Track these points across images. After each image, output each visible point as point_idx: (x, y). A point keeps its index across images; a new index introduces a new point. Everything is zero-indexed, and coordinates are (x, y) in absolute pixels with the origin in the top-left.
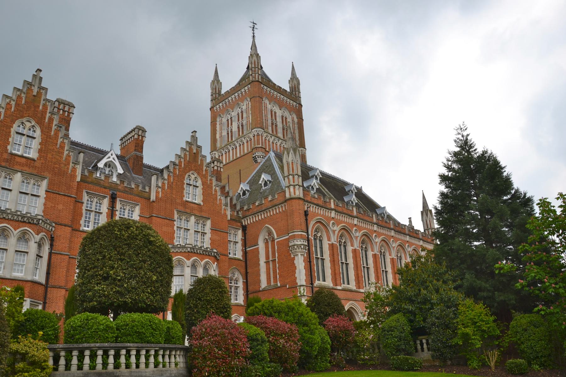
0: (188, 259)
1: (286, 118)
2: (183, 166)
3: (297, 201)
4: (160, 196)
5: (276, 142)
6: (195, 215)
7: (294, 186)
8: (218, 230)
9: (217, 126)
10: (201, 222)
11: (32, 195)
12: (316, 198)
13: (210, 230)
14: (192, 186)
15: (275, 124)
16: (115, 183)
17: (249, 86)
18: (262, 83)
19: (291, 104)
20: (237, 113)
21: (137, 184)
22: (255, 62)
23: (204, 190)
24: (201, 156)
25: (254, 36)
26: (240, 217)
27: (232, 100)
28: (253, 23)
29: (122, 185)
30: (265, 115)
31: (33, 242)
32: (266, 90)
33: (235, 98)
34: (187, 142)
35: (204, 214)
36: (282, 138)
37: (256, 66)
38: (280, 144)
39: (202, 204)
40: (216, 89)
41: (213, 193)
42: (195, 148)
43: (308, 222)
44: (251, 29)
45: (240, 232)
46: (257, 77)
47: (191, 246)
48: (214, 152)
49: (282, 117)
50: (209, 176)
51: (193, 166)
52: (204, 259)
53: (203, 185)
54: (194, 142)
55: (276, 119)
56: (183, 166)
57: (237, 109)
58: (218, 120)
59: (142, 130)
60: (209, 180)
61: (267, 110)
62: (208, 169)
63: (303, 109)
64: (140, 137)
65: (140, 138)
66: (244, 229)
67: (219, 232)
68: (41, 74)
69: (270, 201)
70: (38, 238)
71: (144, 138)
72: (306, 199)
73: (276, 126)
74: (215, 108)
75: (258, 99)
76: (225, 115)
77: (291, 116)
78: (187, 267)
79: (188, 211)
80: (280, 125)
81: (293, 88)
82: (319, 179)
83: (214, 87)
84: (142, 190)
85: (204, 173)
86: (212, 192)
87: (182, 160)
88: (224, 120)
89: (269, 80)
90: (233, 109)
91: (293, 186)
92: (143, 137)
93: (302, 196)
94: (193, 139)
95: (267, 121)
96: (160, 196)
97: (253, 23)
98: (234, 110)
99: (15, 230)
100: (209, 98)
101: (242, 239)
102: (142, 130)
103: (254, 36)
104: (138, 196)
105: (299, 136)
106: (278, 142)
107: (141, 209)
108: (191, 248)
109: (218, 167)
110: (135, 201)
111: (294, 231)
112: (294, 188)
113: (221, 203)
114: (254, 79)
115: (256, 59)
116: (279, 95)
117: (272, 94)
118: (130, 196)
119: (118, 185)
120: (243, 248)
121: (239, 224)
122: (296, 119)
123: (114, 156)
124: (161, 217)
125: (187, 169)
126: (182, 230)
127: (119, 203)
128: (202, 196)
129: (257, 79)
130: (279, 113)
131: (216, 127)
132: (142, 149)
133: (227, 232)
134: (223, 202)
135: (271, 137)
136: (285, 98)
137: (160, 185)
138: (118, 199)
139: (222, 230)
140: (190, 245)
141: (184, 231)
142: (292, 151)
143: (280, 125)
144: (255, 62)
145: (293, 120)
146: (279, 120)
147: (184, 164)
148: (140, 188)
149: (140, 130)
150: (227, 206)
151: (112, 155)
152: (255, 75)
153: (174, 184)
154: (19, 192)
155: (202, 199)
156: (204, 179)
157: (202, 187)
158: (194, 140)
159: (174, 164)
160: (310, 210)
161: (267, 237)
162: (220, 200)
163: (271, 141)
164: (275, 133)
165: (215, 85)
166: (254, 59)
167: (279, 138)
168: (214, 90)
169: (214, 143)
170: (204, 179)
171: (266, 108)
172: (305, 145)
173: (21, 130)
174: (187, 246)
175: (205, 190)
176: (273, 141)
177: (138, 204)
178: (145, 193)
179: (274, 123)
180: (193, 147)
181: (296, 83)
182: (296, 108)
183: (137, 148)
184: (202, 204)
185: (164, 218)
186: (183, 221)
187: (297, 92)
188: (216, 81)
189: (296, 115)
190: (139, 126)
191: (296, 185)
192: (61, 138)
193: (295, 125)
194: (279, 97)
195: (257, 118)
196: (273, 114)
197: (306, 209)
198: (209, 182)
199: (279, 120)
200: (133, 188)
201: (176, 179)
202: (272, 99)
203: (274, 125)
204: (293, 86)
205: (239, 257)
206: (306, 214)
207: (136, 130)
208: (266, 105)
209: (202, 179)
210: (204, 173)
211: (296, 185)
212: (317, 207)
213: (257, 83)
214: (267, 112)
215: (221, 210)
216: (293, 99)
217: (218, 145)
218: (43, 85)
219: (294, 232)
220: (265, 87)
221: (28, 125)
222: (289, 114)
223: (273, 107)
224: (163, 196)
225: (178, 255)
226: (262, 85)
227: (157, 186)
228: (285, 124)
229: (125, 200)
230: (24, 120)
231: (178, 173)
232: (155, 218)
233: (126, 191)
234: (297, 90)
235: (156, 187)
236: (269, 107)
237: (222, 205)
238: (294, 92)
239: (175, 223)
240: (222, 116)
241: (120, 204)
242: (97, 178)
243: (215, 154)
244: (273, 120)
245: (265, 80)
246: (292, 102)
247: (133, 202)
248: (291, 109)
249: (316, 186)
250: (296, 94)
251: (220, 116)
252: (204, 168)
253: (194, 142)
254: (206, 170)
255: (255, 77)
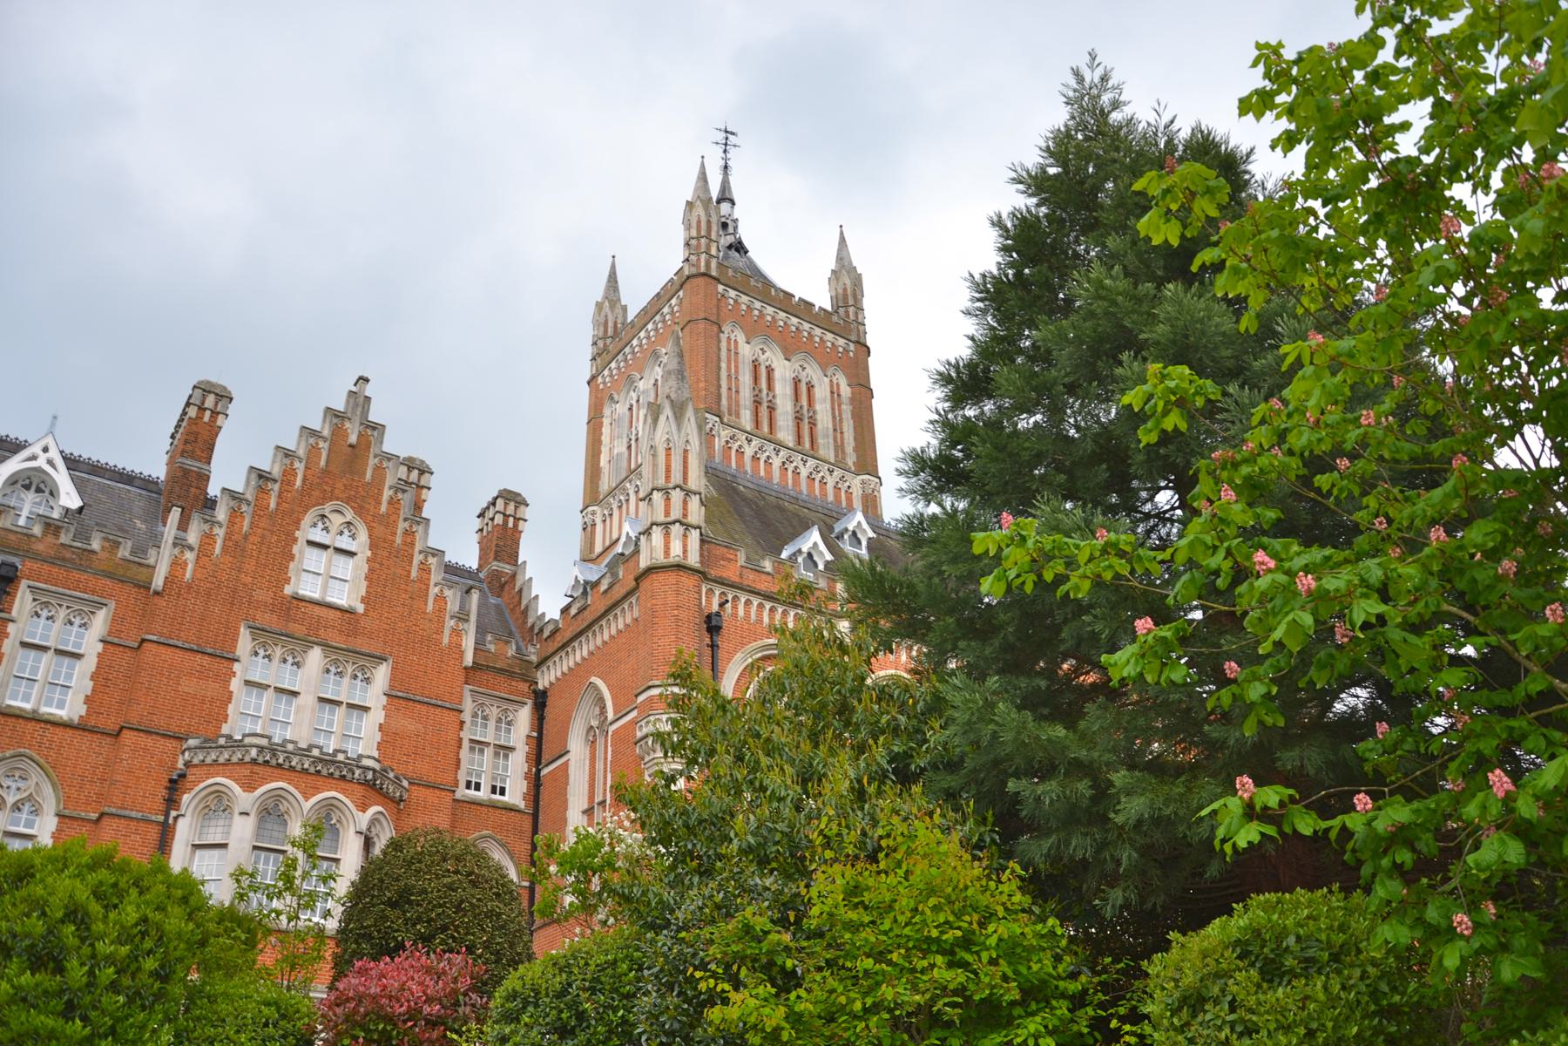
0: (249, 787)
1: (810, 387)
2: (298, 483)
3: (671, 577)
4: (188, 575)
5: (768, 457)
6: (325, 646)
7: (666, 526)
8: (418, 698)
9: (604, 430)
10: (350, 670)
11: (59, 652)
12: (768, 574)
13: (385, 698)
14: (331, 551)
15: (765, 405)
16: (25, 531)
17: (681, 293)
18: (718, 280)
19: (829, 344)
20: (653, 381)
21: (111, 537)
22: (699, 222)
23: (377, 566)
24: (375, 456)
25: (726, 167)
26: (530, 662)
27: (641, 345)
28: (726, 132)
29: (50, 539)
30: (729, 376)
31: (352, 830)
32: (760, 311)
33: (648, 338)
34: (329, 412)
35: (361, 644)
36: (791, 445)
37: (703, 233)
38: (784, 463)
39: (360, 608)
40: (606, 323)
41: (414, 574)
42: (356, 431)
43: (721, 654)
44: (720, 149)
45: (524, 717)
46: (703, 264)
47: (264, 742)
48: (590, 509)
49: (796, 382)
50: (401, 519)
51: (339, 485)
52: (317, 790)
53: (373, 546)
54: (354, 412)
55: (770, 387)
56: (298, 483)
57: (653, 369)
58: (607, 411)
59: (217, 395)
60: (399, 532)
61: (736, 361)
62: (400, 496)
63: (873, 362)
64: (511, 519)
65: (511, 524)
66: (540, 701)
67: (424, 708)
68: (369, 390)
69: (606, 592)
70: (363, 819)
71: (220, 416)
72: (713, 573)
73: (772, 409)
74: (600, 380)
75: (702, 325)
76: (623, 394)
77: (827, 380)
78: (241, 813)
79: (298, 629)
80: (785, 406)
81: (840, 297)
82: (864, 543)
83: (602, 320)
84: (132, 558)
85: (383, 508)
86: (409, 572)
87: (299, 467)
88: (621, 409)
89: (768, 283)
90: (641, 371)
91: (660, 528)
92: (218, 413)
93: (693, 559)
94: (352, 401)
95: (737, 392)
96: (188, 575)
97: (726, 132)
98: (646, 374)
99: (307, 799)
100: (589, 351)
101: (528, 736)
102: (217, 395)
103: (726, 167)
104: (109, 575)
105: (855, 439)
106: (773, 455)
107: (115, 620)
108: (261, 749)
109: (506, 516)
110: (93, 592)
111: (650, 683)
112: (667, 535)
113: (440, 610)
114: (694, 270)
115: (702, 214)
116: (782, 315)
117: (756, 312)
118: (76, 575)
119: (33, 540)
120: (530, 770)
121: (524, 687)
122: (848, 389)
123: (54, 454)
124: (180, 644)
125: (316, 493)
126: (489, 752)
127: (31, 598)
128: (365, 584)
129: (703, 270)
130: (784, 370)
131: (601, 434)
132: (212, 451)
133: (455, 707)
134: (453, 605)
135: (749, 441)
136: (806, 326)
137: (193, 537)
138: (24, 583)
139: (433, 701)
140: (262, 736)
141: (497, 754)
142: (667, 411)
143: (785, 406)
144: (699, 222)
145: (835, 393)
146: (783, 391)
147: (305, 479)
148: (124, 552)
149: (210, 392)
150: (467, 621)
151: (45, 450)
152: (699, 260)
153: (251, 539)
154: (18, 644)
155: (363, 592)
156: (382, 528)
157: (369, 553)
158: (357, 405)
159: (260, 477)
160: (735, 615)
161: (594, 723)
162: (440, 598)
163: (804, 472)
164: (807, 445)
165: (603, 314)
166: (841, 283)
167: (780, 445)
168: (602, 329)
169: (592, 482)
170: (380, 530)
171: (736, 353)
172: (876, 467)
173: (318, 535)
174: (247, 740)
175: (381, 564)
176: (756, 453)
177: (104, 601)
178: (141, 569)
179: (765, 400)
180: (347, 425)
181: (848, 282)
182: (848, 356)
183: (189, 447)
184: (360, 608)
185: (191, 650)
186: (492, 724)
187: (851, 310)
188: (607, 303)
189: (848, 376)
190: (208, 382)
191: (674, 522)
192: (436, 585)
193: (844, 407)
194: (781, 323)
195: (698, 381)
196: (762, 375)
197: (715, 607)
198: (398, 540)
199: (783, 391)
200: (93, 552)
201: (264, 523)
202: (756, 329)
203: (763, 406)
204: (840, 291)
205: (512, 801)
206: (712, 626)
207: (500, 503)
208: (736, 347)
209: (370, 529)
210: (383, 508)
211: (674, 522)
212: (768, 605)
213: (701, 281)
214: (736, 367)
215: (440, 632)
216: (833, 329)
217: (605, 485)
218: (373, 417)
219: (649, 687)
220: (732, 293)
221: (337, 520)
222: (819, 372)
223: (764, 352)
224: (199, 576)
225: (218, 775)
226: (721, 288)
227: (180, 543)
228: (804, 402)
229: (54, 588)
230: (327, 508)
231: (273, 505)
232: (155, 645)
233: (64, 559)
234: (851, 302)
235: (175, 545)
236: (746, 351)
237: (447, 618)
238: (841, 311)
239: (236, 667)
240: (616, 397)
241: (35, 600)
242: (15, 529)
243: (594, 513)
244: (760, 391)
245: (730, 273)
246: (829, 336)
247: (86, 596)
248: (826, 360)
249: (821, 553)
250: (848, 316)
251: (611, 398)
252: (387, 494)
253: (354, 412)
254: (391, 502)
255: (697, 265)
